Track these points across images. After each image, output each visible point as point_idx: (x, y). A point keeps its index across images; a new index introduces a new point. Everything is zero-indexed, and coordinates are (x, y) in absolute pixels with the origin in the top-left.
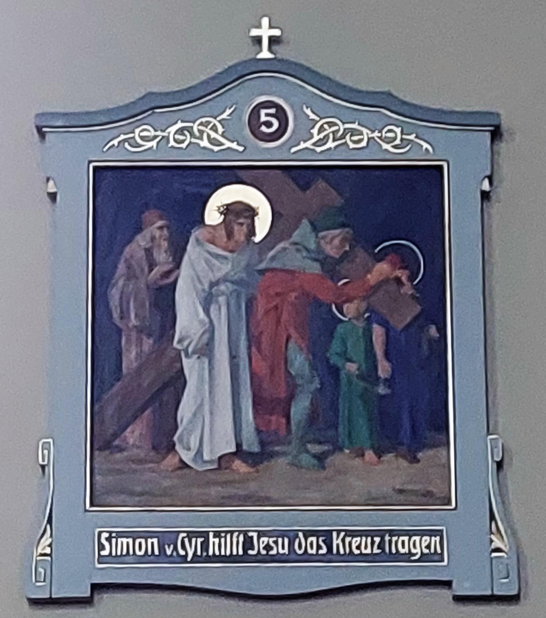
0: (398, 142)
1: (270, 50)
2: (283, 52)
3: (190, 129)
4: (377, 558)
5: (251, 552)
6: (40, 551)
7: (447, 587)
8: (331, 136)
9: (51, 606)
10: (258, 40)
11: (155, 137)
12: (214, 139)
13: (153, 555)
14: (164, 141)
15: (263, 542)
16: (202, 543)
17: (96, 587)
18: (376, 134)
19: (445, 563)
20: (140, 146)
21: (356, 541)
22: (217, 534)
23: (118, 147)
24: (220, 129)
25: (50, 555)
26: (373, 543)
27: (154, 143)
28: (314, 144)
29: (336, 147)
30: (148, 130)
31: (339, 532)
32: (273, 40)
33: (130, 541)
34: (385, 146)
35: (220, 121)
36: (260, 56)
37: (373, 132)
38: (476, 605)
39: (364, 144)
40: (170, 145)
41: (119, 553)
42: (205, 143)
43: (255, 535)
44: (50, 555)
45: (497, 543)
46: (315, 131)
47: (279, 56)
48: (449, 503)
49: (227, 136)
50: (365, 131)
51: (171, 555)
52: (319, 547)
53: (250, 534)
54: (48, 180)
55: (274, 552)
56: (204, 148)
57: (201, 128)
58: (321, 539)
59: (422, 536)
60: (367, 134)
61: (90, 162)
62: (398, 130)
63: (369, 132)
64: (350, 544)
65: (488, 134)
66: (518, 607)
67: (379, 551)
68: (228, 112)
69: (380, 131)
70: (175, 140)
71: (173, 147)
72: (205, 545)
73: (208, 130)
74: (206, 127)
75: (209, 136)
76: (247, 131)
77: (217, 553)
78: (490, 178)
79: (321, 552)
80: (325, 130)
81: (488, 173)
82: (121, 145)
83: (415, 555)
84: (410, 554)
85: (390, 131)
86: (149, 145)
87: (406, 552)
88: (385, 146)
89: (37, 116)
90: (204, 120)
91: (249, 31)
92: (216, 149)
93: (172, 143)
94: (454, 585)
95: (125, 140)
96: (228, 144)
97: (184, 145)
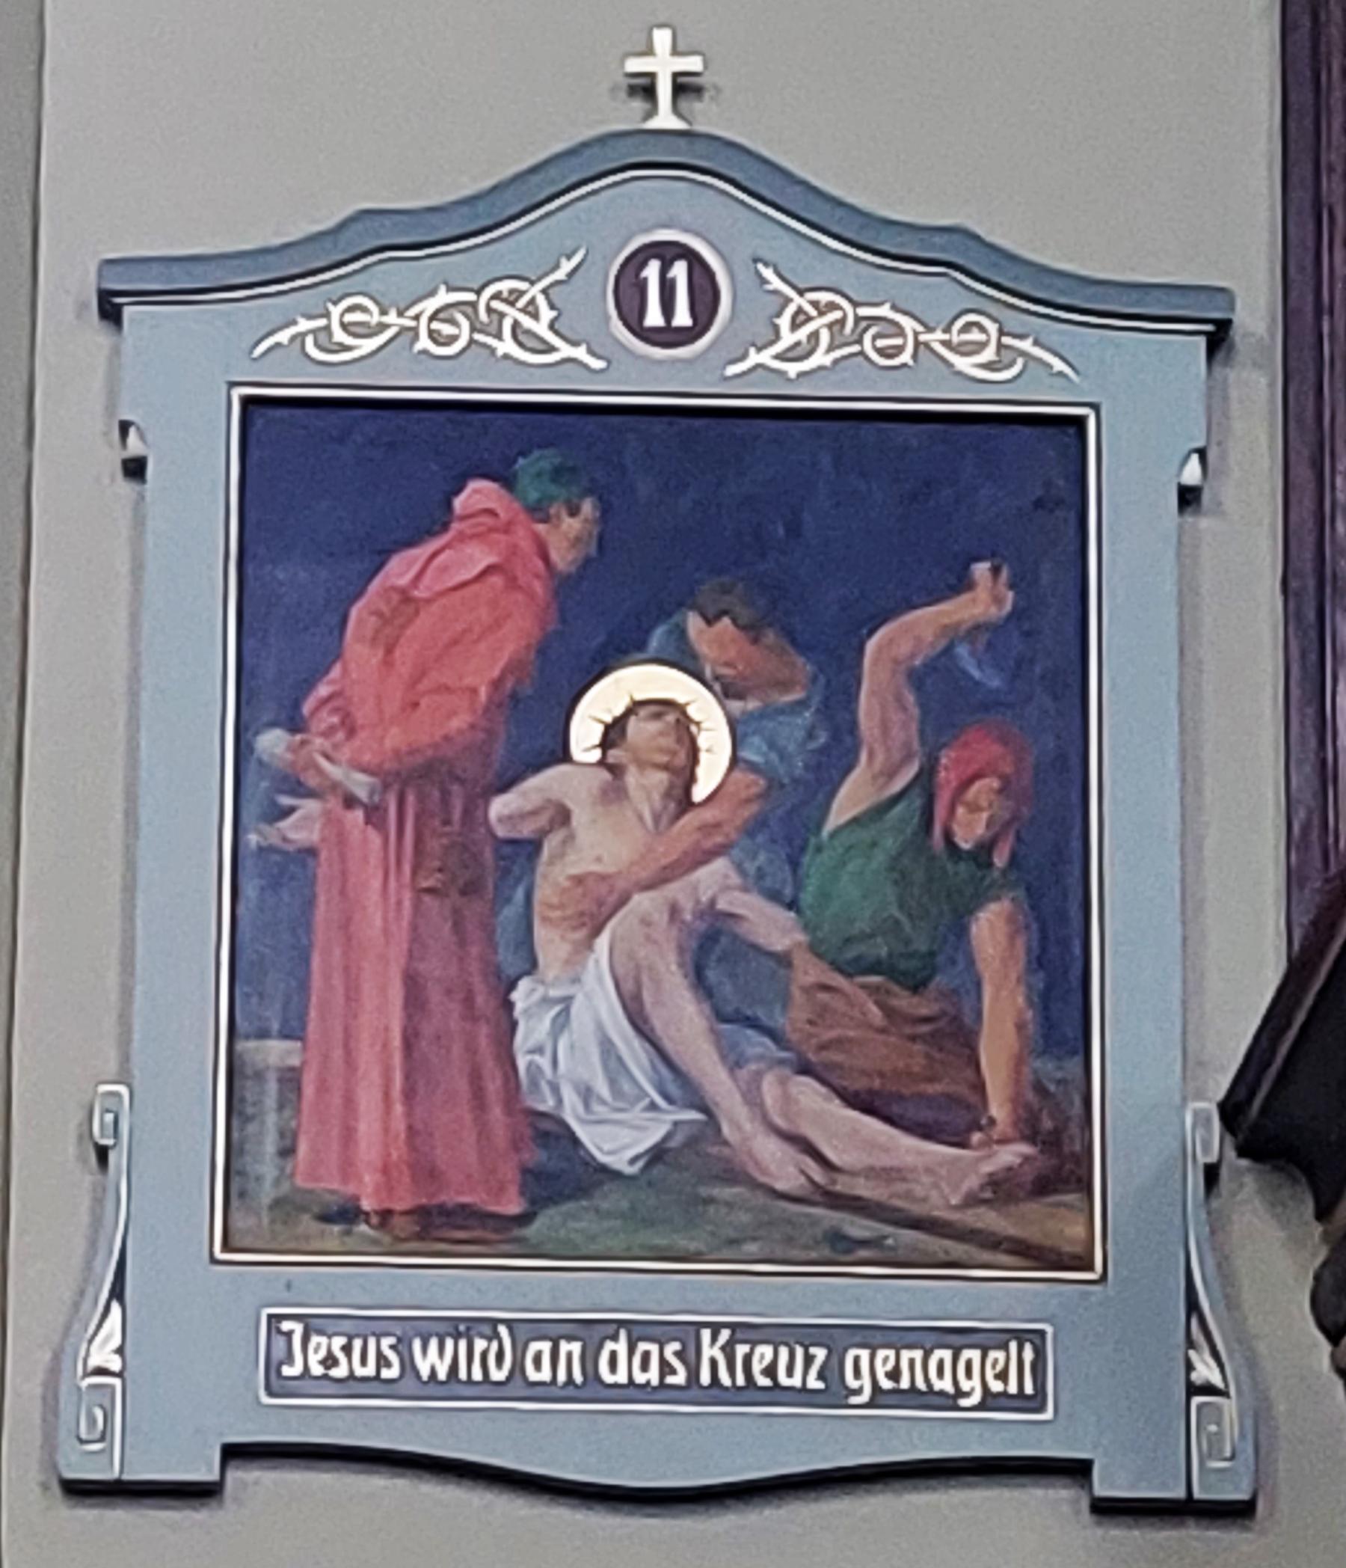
2: (707, 118)
3: (864, 324)
4: (819, 1399)
5: (287, 1371)
8: (825, 337)
9: (626, 1507)
10: (645, 88)
11: (383, 327)
12: (529, 332)
17: (232, 1453)
18: (935, 338)
19: (266, 1400)
20: (348, 348)
21: (764, 1353)
23: (1052, 375)
24: (547, 314)
25: (119, 1375)
26: (809, 1359)
28: (778, 357)
29: (836, 362)
30: (364, 309)
31: (716, 1328)
32: (684, 87)
33: (918, 1355)
34: (962, 363)
36: (654, 124)
37: (930, 329)
39: (906, 357)
40: (911, 362)
42: (507, 346)
43: (298, 1328)
44: (119, 1375)
45: (1206, 1371)
46: (784, 322)
47: (700, 128)
48: (1090, 1267)
49: (563, 331)
50: (908, 324)
52: (382, 1361)
53: (286, 1326)
54: (124, 427)
55: (340, 1372)
57: (496, 304)
59: (754, 1344)
60: (916, 334)
63: (920, 328)
64: (748, 1360)
65: (1201, 342)
66: (221, 1513)
67: (820, 1385)
68: (567, 266)
69: (947, 330)
70: (433, 335)
71: (425, 352)
72: (690, 1357)
73: (512, 313)
74: (512, 304)
75: (516, 325)
77: (921, 1384)
78: (1202, 453)
79: (386, 1374)
81: (1200, 443)
83: (858, 1392)
84: (960, 1393)
85: (967, 328)
88: (962, 363)
90: (505, 286)
91: (622, 64)
93: (424, 343)
96: (566, 351)
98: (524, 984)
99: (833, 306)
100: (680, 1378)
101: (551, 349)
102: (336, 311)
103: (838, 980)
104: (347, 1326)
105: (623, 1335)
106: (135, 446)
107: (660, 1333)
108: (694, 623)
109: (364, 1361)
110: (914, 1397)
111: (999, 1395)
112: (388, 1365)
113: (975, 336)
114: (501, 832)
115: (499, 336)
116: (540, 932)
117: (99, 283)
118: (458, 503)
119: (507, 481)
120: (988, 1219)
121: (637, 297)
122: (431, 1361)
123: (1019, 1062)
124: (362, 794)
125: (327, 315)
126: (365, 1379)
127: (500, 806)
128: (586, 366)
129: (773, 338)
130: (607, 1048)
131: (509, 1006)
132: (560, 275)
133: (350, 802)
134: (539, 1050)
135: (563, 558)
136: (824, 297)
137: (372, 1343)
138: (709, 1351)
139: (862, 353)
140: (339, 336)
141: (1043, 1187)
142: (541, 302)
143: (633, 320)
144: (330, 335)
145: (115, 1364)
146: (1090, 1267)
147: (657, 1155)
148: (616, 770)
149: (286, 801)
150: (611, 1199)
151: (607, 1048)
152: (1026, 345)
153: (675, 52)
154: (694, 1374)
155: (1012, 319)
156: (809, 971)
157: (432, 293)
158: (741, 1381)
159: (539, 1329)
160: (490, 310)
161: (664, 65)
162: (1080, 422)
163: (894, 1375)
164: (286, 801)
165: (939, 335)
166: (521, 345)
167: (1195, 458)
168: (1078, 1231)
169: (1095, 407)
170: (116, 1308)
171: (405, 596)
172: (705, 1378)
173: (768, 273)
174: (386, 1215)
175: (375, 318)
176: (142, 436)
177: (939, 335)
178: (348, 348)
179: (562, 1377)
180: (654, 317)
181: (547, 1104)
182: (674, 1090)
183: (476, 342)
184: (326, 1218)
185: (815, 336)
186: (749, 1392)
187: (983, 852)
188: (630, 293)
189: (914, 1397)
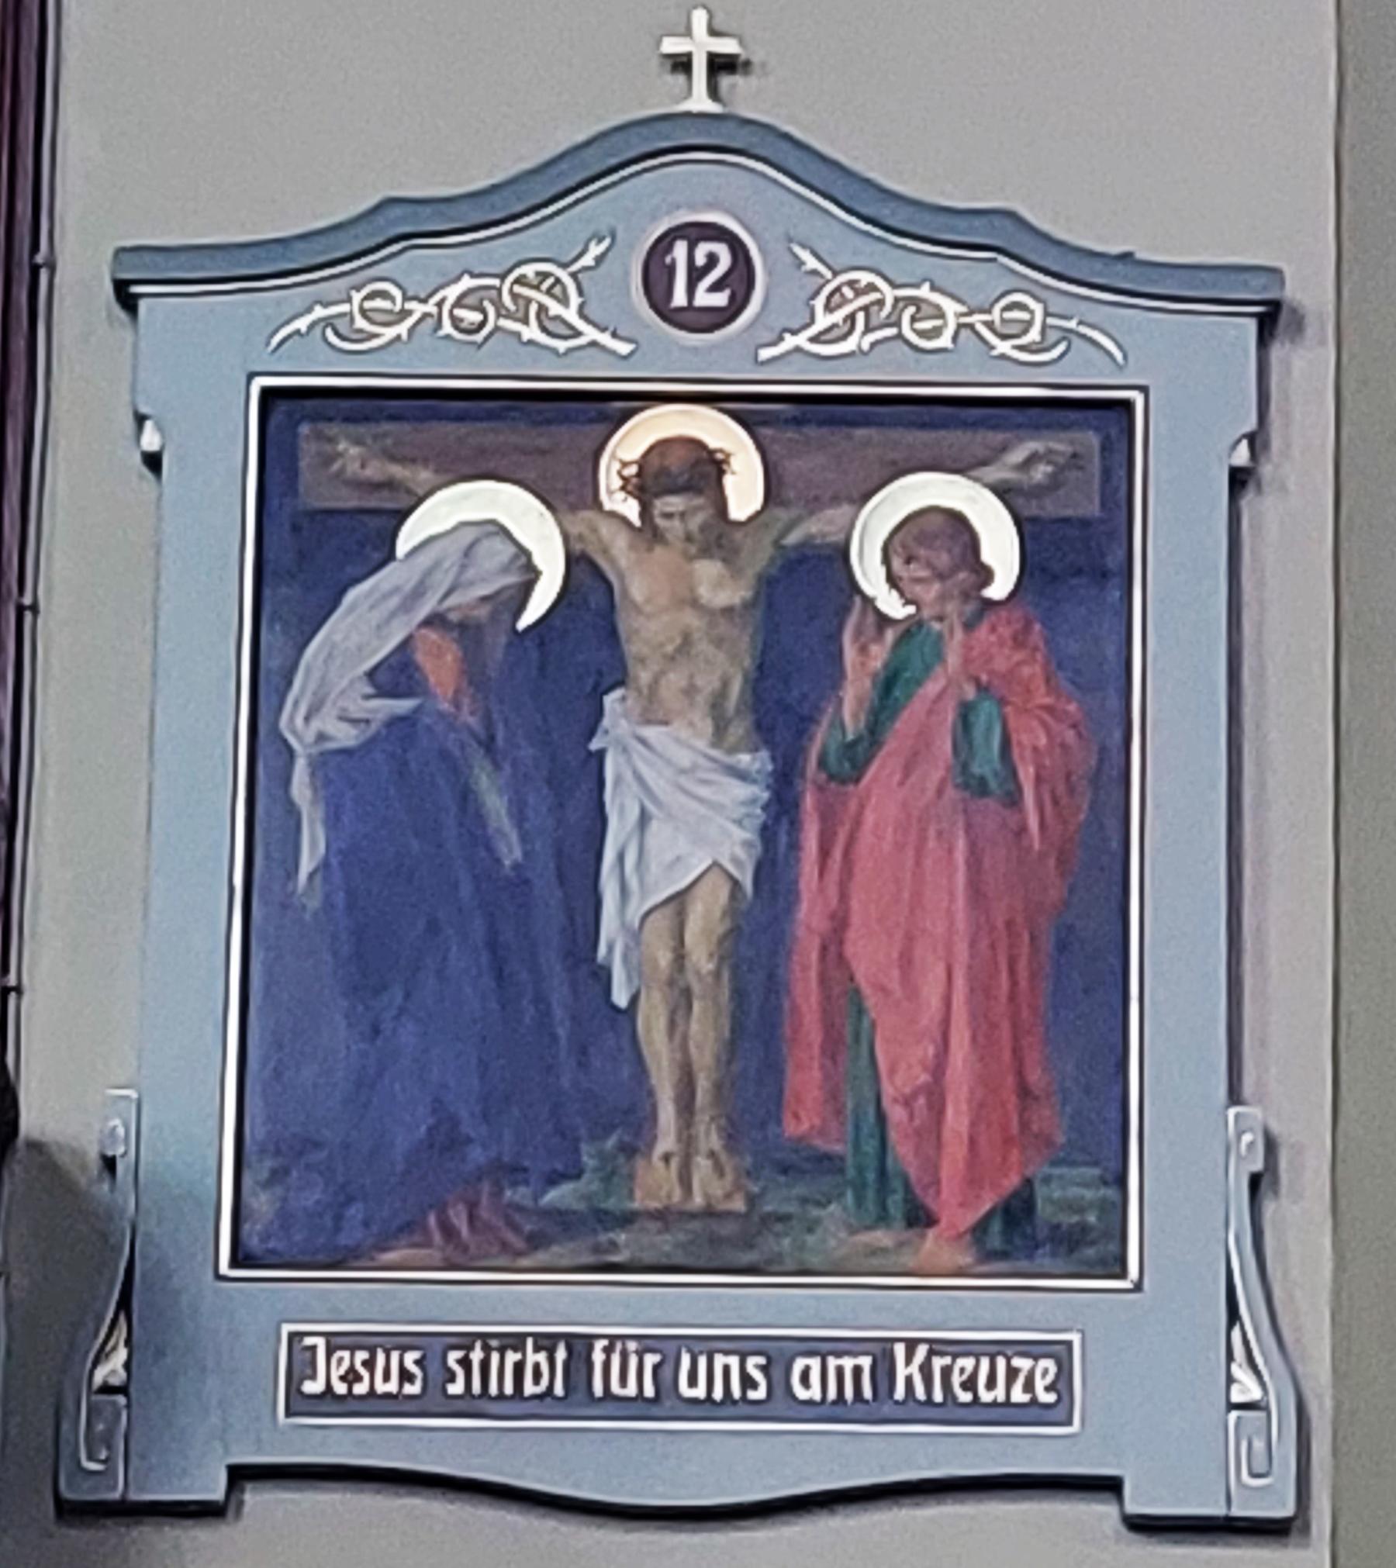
0: (1034, 335)
1: (714, 93)
7: (1107, 1495)
8: (861, 317)
10: (682, 64)
11: (405, 314)
12: (558, 318)
13: (517, 1397)
14: (430, 322)
15: (962, 1370)
16: (656, 1368)
17: (240, 1475)
22: (545, 1342)
27: (402, 329)
28: (814, 340)
32: (719, 65)
34: (1004, 347)
35: (574, 276)
38: (1160, 1543)
39: (945, 341)
40: (441, 333)
41: (493, 1389)
43: (320, 1342)
46: (819, 303)
48: (1123, 1274)
50: (950, 307)
51: (501, 1396)
52: (406, 1376)
53: (309, 1341)
54: (140, 420)
56: (531, 342)
58: (752, 1362)
59: (955, 1356)
61: (251, 376)
64: (947, 1372)
65: (1252, 325)
67: (1050, 1398)
70: (456, 322)
71: (448, 337)
72: (777, 1363)
74: (537, 288)
75: (542, 309)
78: (1251, 438)
79: (752, 1395)
80: (845, 301)
82: (318, 330)
86: (389, 333)
87: (996, 1399)
89: (120, 251)
92: (561, 345)
93: (447, 328)
94: (1127, 1490)
95: (328, 322)
97: (479, 337)
99: (872, 288)
102: (357, 297)
105: (478, 1345)
106: (150, 440)
109: (387, 1377)
111: (341, 1398)
112: (754, 1385)
115: (525, 321)
117: (113, 272)
121: (665, 278)
125: (349, 300)
126: (388, 1396)
128: (613, 353)
129: (808, 321)
132: (588, 260)
137: (395, 1356)
139: (899, 336)
140: (360, 323)
144: (352, 320)
146: (1123, 1274)
155: (1058, 304)
158: (938, 1396)
160: (515, 297)
161: (700, 45)
166: (544, 329)
167: (1244, 443)
169: (1144, 389)
170: (122, 1319)
172: (900, 1393)
173: (805, 255)
176: (160, 428)
178: (376, 336)
179: (718, 1394)
183: (342, 302)
185: (851, 318)
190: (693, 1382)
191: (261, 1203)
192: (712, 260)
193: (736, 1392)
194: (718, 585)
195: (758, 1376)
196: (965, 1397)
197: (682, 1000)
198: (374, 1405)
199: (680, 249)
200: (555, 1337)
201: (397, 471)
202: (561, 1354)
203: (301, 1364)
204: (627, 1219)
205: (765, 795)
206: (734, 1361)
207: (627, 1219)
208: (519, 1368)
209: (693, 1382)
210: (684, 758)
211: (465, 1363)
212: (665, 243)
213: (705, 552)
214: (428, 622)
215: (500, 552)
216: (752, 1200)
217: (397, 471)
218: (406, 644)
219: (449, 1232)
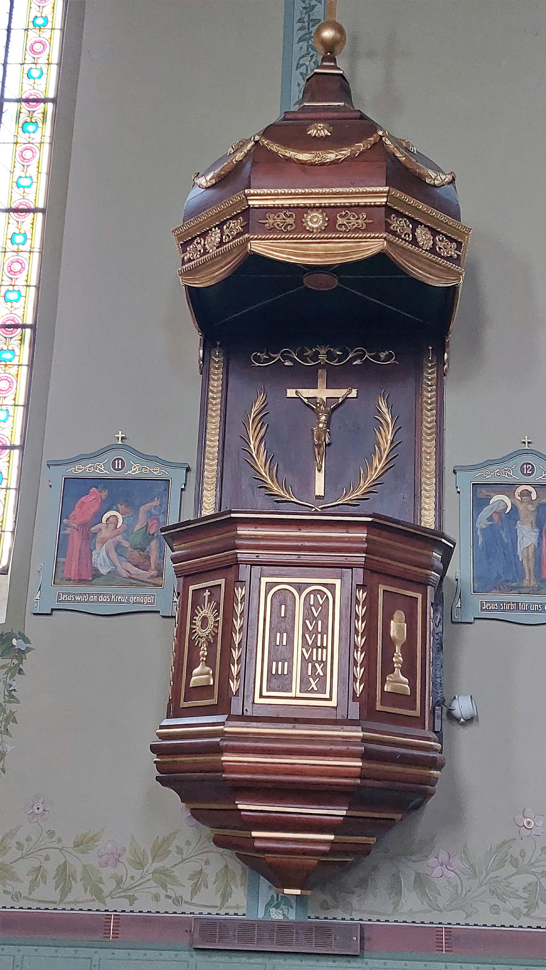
1: (121, 441)
2: (126, 442)
5: (60, 599)
6: (36, 598)
8: (138, 469)
10: (524, 443)
11: (491, 474)
17: (52, 610)
24: (103, 467)
25: (460, 608)
27: (490, 476)
28: (132, 472)
31: (114, 594)
32: (529, 443)
34: (154, 473)
39: (148, 472)
42: (98, 471)
43: (485, 602)
47: (124, 444)
54: (457, 487)
62: (159, 468)
64: (118, 598)
68: (106, 461)
72: (529, 606)
76: (520, 473)
79: (540, 610)
86: (488, 477)
88: (154, 473)
89: (48, 461)
92: (510, 478)
93: (87, 471)
96: (105, 471)
98: (94, 551)
100: (109, 600)
101: (103, 471)
102: (77, 467)
103: (133, 550)
104: (122, 595)
107: (106, 595)
108: (119, 505)
110: (137, 603)
113: (157, 469)
114: (93, 532)
116: (97, 544)
118: (91, 491)
119: (97, 488)
120: (150, 581)
122: (78, 598)
123: (156, 561)
124: (76, 527)
127: (93, 529)
130: (104, 559)
131: (92, 554)
132: (105, 462)
133: (74, 528)
134: (95, 559)
135: (103, 498)
136: (138, 465)
138: (113, 597)
140: (485, 475)
141: (157, 576)
142: (102, 465)
143: (114, 468)
145: (39, 599)
147: (109, 572)
148: (108, 524)
149: (66, 528)
150: (102, 578)
151: (104, 559)
152: (163, 471)
153: (122, 434)
154: (110, 600)
156: (130, 549)
157: (89, 464)
159: (92, 594)
161: (120, 435)
162: (169, 480)
163: (136, 600)
164: (66, 528)
165: (152, 469)
168: (161, 582)
171: (83, 503)
172: (112, 601)
174: (74, 580)
175: (82, 468)
177: (152, 469)
180: (116, 467)
181: (96, 566)
182: (112, 564)
184: (67, 580)
186: (117, 602)
187: (153, 535)
188: (114, 465)
189: (137, 603)
190: (532, 608)
191: (476, 585)
192: (529, 467)
193: (538, 609)
194: (531, 508)
195: (540, 608)
196: (487, 608)
197: (528, 560)
198: (492, 610)
199: (525, 466)
200: (514, 602)
201: (489, 493)
202: (515, 604)
203: (482, 605)
204: (522, 588)
205: (538, 534)
206: (537, 606)
207: (522, 588)
208: (510, 606)
209: (532, 608)
210: (528, 530)
211: (503, 605)
212: (523, 465)
213: (529, 504)
214: (494, 512)
215: (502, 504)
216: (538, 586)
217: (489, 493)
218: (491, 515)
219: (500, 589)
